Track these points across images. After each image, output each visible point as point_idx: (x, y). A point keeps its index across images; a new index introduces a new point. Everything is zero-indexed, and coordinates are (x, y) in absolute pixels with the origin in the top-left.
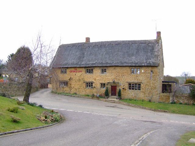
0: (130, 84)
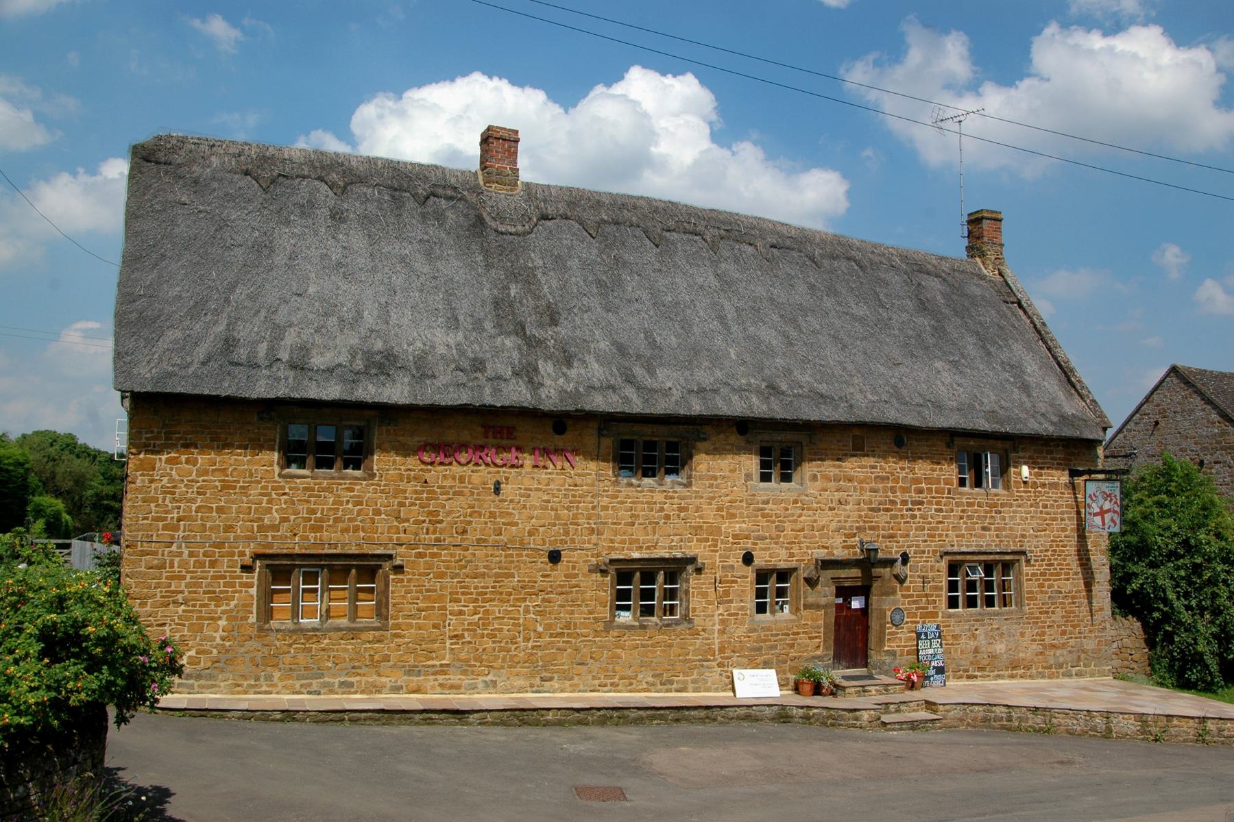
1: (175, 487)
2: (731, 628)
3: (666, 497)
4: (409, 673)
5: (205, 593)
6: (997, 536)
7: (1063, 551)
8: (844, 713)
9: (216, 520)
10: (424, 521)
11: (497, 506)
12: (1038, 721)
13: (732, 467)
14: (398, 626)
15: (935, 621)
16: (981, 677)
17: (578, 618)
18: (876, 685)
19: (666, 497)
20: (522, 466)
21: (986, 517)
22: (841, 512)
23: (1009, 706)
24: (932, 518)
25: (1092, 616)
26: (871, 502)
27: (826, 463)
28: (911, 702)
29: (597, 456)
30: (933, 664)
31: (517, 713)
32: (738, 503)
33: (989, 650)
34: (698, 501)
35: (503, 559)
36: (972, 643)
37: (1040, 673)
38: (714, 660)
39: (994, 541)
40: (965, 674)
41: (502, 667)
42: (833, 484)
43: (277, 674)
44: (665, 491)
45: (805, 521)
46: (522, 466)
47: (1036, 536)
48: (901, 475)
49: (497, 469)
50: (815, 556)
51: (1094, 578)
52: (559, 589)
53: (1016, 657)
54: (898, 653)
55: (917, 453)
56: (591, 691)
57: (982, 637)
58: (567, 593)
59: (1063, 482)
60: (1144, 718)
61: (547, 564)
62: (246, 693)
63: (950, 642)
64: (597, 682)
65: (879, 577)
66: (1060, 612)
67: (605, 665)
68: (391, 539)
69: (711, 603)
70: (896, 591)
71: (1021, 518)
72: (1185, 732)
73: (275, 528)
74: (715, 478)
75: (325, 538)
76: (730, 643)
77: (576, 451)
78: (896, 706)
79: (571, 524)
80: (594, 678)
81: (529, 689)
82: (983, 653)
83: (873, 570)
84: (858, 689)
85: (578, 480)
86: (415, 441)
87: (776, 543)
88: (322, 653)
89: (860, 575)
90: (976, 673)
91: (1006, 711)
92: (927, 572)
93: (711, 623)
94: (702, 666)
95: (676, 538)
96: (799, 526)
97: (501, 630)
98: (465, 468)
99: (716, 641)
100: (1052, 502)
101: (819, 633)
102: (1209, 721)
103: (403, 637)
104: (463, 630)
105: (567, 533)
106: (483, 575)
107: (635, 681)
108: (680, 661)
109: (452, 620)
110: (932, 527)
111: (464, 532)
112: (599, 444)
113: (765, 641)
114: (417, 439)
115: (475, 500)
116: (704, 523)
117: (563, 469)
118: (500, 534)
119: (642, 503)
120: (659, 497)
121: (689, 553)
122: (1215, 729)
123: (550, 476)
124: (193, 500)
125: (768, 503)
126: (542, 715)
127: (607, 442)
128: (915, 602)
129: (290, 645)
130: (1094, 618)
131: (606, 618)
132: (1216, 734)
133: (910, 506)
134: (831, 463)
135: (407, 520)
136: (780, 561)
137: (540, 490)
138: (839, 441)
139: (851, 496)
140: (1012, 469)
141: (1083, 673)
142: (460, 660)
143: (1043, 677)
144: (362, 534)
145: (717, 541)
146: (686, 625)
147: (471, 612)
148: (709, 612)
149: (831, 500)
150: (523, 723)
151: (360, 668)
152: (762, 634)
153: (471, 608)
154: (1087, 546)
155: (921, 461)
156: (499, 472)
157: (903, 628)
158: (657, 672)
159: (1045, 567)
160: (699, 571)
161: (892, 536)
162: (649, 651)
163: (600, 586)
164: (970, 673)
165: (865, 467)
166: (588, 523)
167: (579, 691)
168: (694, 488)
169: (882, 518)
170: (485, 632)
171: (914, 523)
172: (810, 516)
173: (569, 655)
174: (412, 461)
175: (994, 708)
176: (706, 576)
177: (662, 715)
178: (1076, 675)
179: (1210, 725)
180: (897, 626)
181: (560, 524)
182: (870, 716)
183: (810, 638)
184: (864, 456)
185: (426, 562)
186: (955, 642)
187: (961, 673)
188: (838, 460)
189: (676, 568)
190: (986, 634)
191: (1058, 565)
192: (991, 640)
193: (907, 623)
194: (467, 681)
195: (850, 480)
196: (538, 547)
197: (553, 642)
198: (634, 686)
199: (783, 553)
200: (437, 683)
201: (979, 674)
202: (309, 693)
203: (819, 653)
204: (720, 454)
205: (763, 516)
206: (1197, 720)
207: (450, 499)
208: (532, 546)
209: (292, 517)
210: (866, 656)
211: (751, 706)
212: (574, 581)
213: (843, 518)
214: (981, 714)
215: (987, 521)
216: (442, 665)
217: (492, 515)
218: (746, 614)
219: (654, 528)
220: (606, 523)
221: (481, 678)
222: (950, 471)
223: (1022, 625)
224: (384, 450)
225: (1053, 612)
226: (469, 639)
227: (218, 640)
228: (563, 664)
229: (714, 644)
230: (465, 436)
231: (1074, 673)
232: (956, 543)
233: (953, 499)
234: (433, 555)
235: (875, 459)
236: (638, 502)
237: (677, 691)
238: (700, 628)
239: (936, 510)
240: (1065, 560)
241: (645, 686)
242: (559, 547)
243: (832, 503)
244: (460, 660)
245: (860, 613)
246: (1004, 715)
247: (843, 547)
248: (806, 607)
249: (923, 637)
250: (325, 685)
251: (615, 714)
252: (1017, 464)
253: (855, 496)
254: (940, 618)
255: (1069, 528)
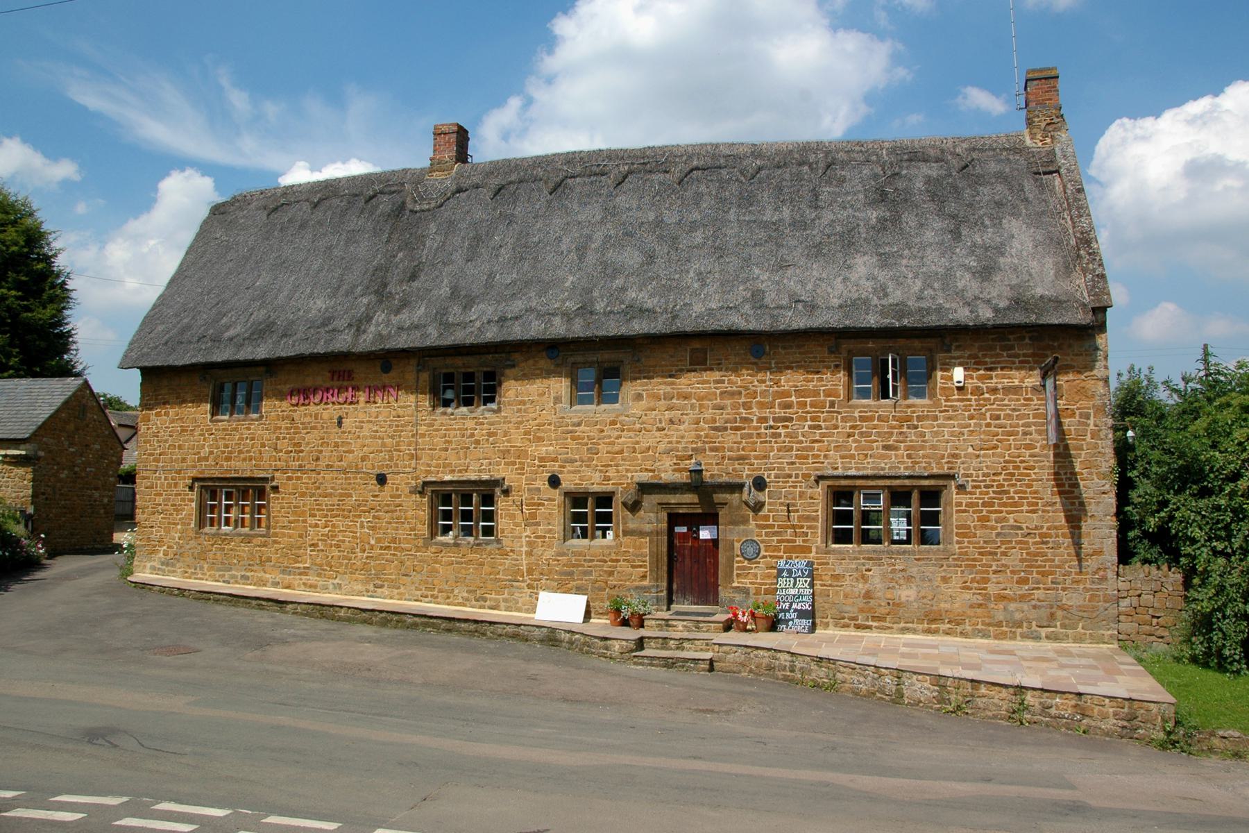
0: (841, 495)
1: (158, 432)
2: (539, 550)
3: (476, 424)
4: (283, 572)
5: (172, 505)
6: (909, 456)
7: (1028, 475)
8: (596, 640)
9: (178, 455)
10: (291, 451)
11: (339, 437)
12: (822, 674)
13: (541, 392)
14: (276, 535)
15: (806, 557)
16: (877, 628)
17: (402, 534)
18: (684, 620)
19: (476, 424)
20: (358, 402)
21: (892, 433)
22: (672, 433)
23: (793, 654)
24: (804, 436)
25: (1080, 561)
26: (714, 421)
27: (655, 380)
28: (698, 640)
29: (416, 390)
30: (794, 606)
31: (318, 607)
32: (546, 426)
33: (889, 596)
34: (506, 426)
35: (344, 481)
36: (861, 586)
37: (980, 631)
38: (523, 581)
39: (903, 463)
40: (853, 622)
41: (345, 573)
42: (663, 402)
43: (206, 566)
44: (476, 418)
45: (624, 443)
46: (358, 402)
47: (978, 456)
48: (759, 389)
49: (340, 406)
50: (636, 479)
51: (1085, 511)
52: (386, 508)
53: (934, 608)
54: (752, 591)
55: (784, 363)
56: (416, 600)
57: (877, 580)
58: (392, 511)
59: (1031, 385)
60: (942, 681)
61: (376, 486)
62: (190, 578)
63: (827, 583)
64: (419, 593)
65: (726, 504)
66: (1016, 556)
67: (425, 578)
68: (271, 465)
69: (517, 525)
70: (748, 520)
71: (952, 434)
72: (996, 705)
73: (206, 459)
74: (523, 402)
75: (233, 466)
76: (538, 565)
77: (399, 387)
78: (677, 643)
79: (395, 450)
80: (417, 589)
81: (365, 593)
82: (879, 598)
83: (714, 495)
84: (660, 622)
85: (400, 412)
86: (286, 388)
87: (588, 466)
88: (231, 552)
89: (696, 500)
90: (871, 623)
91: (790, 659)
92: (794, 499)
93: (519, 544)
94: (512, 586)
95: (485, 462)
96: (617, 448)
97: (343, 541)
98: (319, 407)
99: (524, 562)
100: (1008, 412)
101: (644, 562)
102: (1030, 693)
103: (279, 543)
104: (318, 540)
105: (391, 459)
106: (331, 495)
107: (452, 595)
108: (491, 579)
109: (311, 531)
110: (803, 448)
111: (318, 459)
112: (418, 378)
113: (578, 566)
114: (288, 386)
115: (324, 432)
116: (511, 446)
117: (388, 403)
118: (341, 460)
119: (455, 429)
120: (470, 424)
121: (497, 476)
122: (1037, 704)
123: (378, 410)
124: (166, 441)
125: (579, 424)
126: (337, 612)
127: (425, 376)
128: (774, 534)
129: (212, 545)
130: (1084, 564)
131: (424, 535)
132: (1039, 712)
133: (771, 423)
134: (660, 380)
135: (281, 451)
136: (593, 484)
137: (371, 422)
138: (672, 356)
139: (686, 414)
140: (939, 374)
141: (1061, 636)
142: (316, 564)
143: (984, 636)
144: (254, 462)
145: (524, 464)
146: (495, 545)
147: (323, 526)
148: (517, 533)
149: (660, 420)
150: (323, 616)
151: (253, 565)
152: (573, 559)
153: (323, 522)
154: (1073, 467)
155: (789, 371)
156: (341, 409)
157: (759, 563)
158: (471, 588)
159: (992, 495)
160: (506, 492)
161: (741, 458)
162: (463, 568)
163: (418, 506)
164: (859, 622)
165: (708, 382)
166: (409, 450)
167: (405, 600)
168: (503, 414)
169: (729, 438)
170: (333, 542)
171: (776, 442)
172: (630, 437)
173: (396, 567)
174: (285, 405)
175: (779, 655)
176: (514, 496)
177: (433, 623)
178: (1047, 637)
179: (1029, 698)
180: (749, 560)
181: (385, 451)
182: (622, 647)
183: (633, 567)
184: (706, 370)
185: (293, 484)
186: (835, 583)
187: (846, 620)
188: (671, 376)
189: (488, 491)
190: (883, 575)
191: (1016, 492)
192: (891, 581)
193: (765, 557)
194: (321, 583)
195: (686, 398)
196: (369, 471)
197: (382, 554)
198: (451, 600)
199: (597, 477)
200: (301, 582)
201: (874, 624)
202: (224, 582)
203: (646, 583)
204: (529, 379)
205: (573, 438)
206: (1011, 690)
207: (308, 433)
208: (364, 470)
209: (216, 450)
210: (716, 593)
211: (520, 625)
212: (398, 501)
213: (675, 439)
214: (766, 661)
215: (894, 438)
216: (304, 568)
217: (337, 445)
218: (554, 538)
219: (466, 453)
220: (423, 449)
221: (331, 581)
222: (836, 381)
223: (945, 567)
224: (269, 397)
225: (1004, 554)
226: (322, 548)
227: (177, 540)
228: (391, 574)
229: (522, 566)
230: (319, 381)
231: (1043, 635)
232: (840, 465)
233: (839, 413)
234: (298, 478)
235: (721, 373)
236: (451, 429)
237: (491, 608)
238: (508, 549)
239: (810, 427)
240: (1031, 486)
241: (461, 600)
242: (385, 471)
243: (661, 423)
244: (316, 564)
245: (711, 544)
246: (788, 664)
247: (674, 470)
248: (626, 533)
249: (785, 574)
250: (233, 577)
251: (395, 618)
252: (948, 367)
253: (693, 415)
254: (813, 554)
255: (1038, 445)
